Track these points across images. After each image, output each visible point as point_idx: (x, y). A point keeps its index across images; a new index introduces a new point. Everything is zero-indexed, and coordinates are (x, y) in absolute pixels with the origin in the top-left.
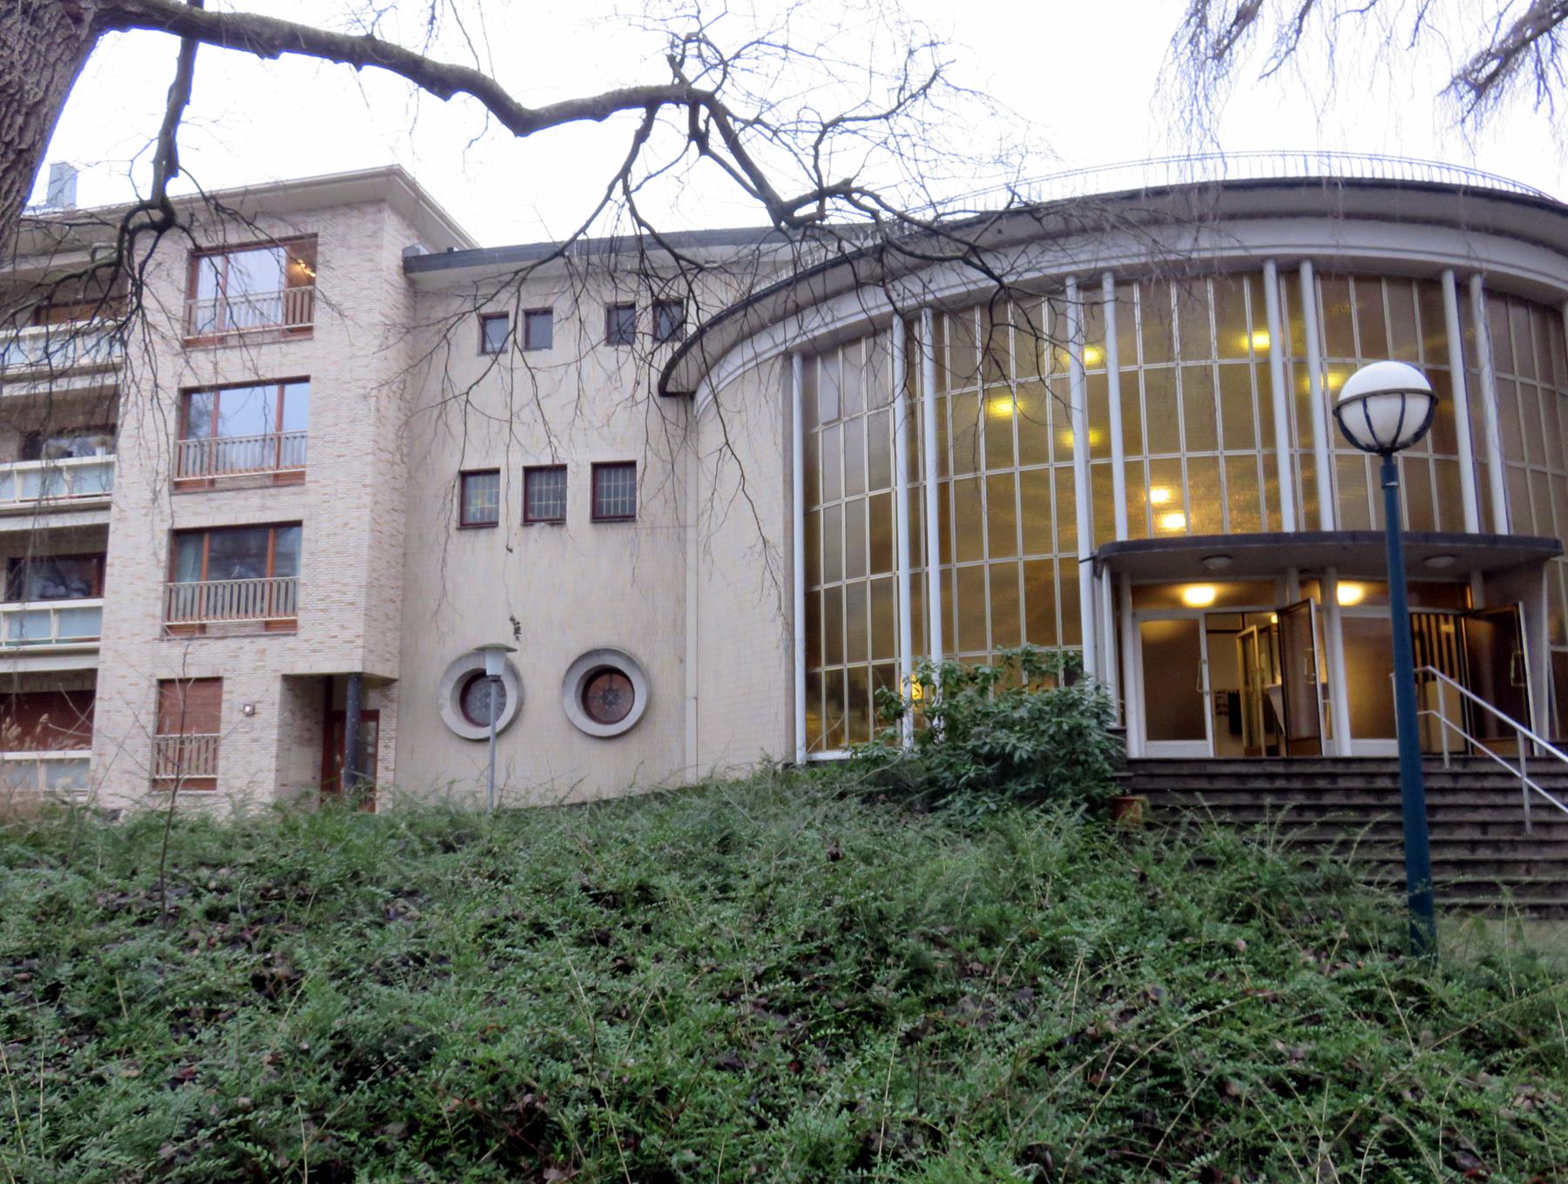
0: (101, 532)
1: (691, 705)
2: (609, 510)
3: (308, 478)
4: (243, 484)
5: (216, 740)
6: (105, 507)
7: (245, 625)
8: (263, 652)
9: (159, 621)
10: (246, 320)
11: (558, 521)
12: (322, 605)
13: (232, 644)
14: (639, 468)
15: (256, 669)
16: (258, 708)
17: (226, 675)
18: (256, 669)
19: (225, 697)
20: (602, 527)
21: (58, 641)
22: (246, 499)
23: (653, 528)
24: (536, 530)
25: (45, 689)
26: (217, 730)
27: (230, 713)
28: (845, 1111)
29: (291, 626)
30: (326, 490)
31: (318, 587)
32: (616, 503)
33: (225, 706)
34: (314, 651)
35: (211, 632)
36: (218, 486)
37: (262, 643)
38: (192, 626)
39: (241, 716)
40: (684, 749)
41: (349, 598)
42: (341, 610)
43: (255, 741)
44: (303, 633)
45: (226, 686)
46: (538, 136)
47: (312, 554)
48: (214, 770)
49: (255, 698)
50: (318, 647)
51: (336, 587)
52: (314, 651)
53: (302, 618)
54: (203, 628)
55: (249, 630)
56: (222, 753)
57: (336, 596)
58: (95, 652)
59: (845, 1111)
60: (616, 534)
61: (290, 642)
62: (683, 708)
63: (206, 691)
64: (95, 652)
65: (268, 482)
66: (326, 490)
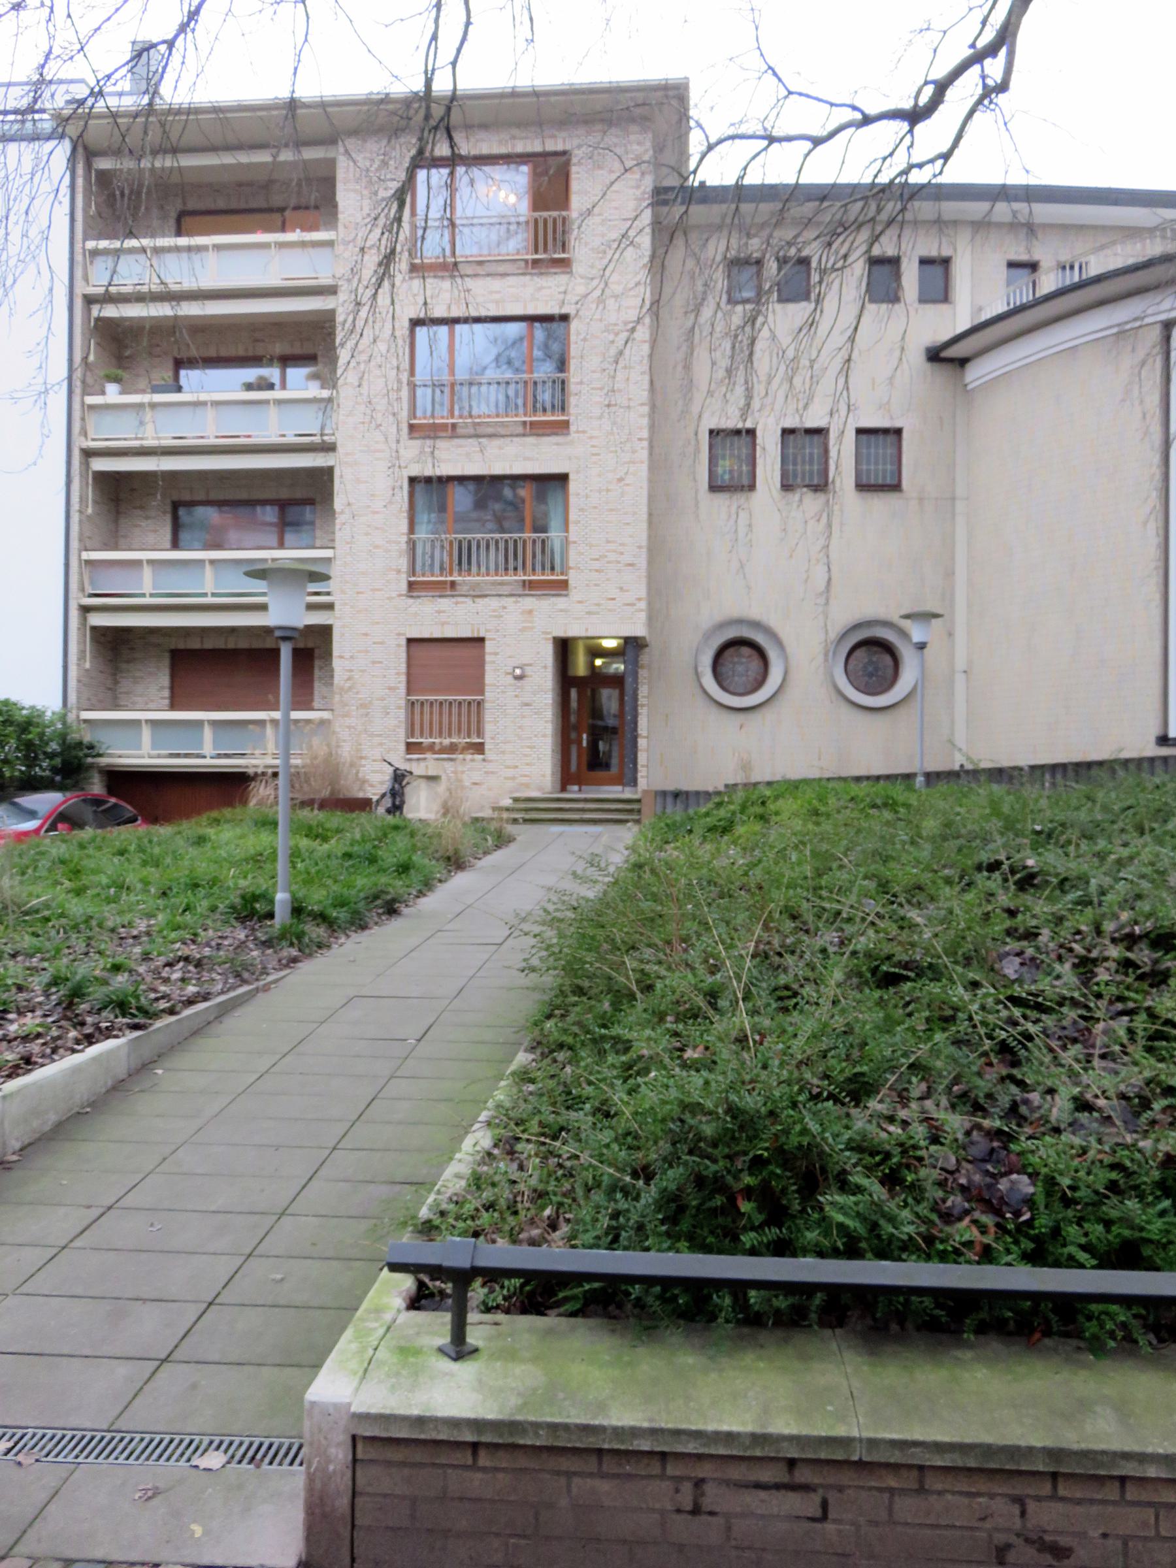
0: (326, 475)
1: (960, 678)
2: (868, 477)
3: (573, 428)
4: (502, 431)
5: (479, 704)
6: (330, 448)
7: (502, 584)
8: (530, 612)
9: (404, 576)
10: (469, 246)
11: (821, 486)
12: (597, 565)
13: (494, 603)
14: (833, 435)
15: (523, 630)
16: (528, 670)
17: (487, 636)
18: (523, 630)
19: (488, 658)
20: (868, 495)
21: (152, 595)
22: (500, 448)
23: (921, 500)
24: (795, 497)
25: (231, 646)
26: (482, 692)
27: (495, 675)
28: (612, 1113)
29: (562, 586)
30: (595, 442)
31: (591, 546)
32: (876, 471)
33: (488, 667)
34: (589, 613)
35: (463, 589)
36: (460, 431)
37: (529, 602)
38: (445, 582)
39: (510, 679)
40: (953, 722)
41: (627, 558)
42: (619, 571)
43: (527, 705)
44: (575, 593)
45: (489, 646)
46: (1013, 84)
47: (581, 510)
48: (480, 733)
49: (525, 660)
50: (594, 608)
51: (612, 546)
52: (589, 613)
53: (573, 577)
54: (453, 584)
55: (506, 590)
56: (488, 716)
57: (612, 557)
58: (330, 607)
59: (612, 1113)
60: (880, 503)
61: (560, 602)
62: (951, 682)
63: (468, 651)
64: (330, 607)
65: (520, 430)
66: (595, 442)
